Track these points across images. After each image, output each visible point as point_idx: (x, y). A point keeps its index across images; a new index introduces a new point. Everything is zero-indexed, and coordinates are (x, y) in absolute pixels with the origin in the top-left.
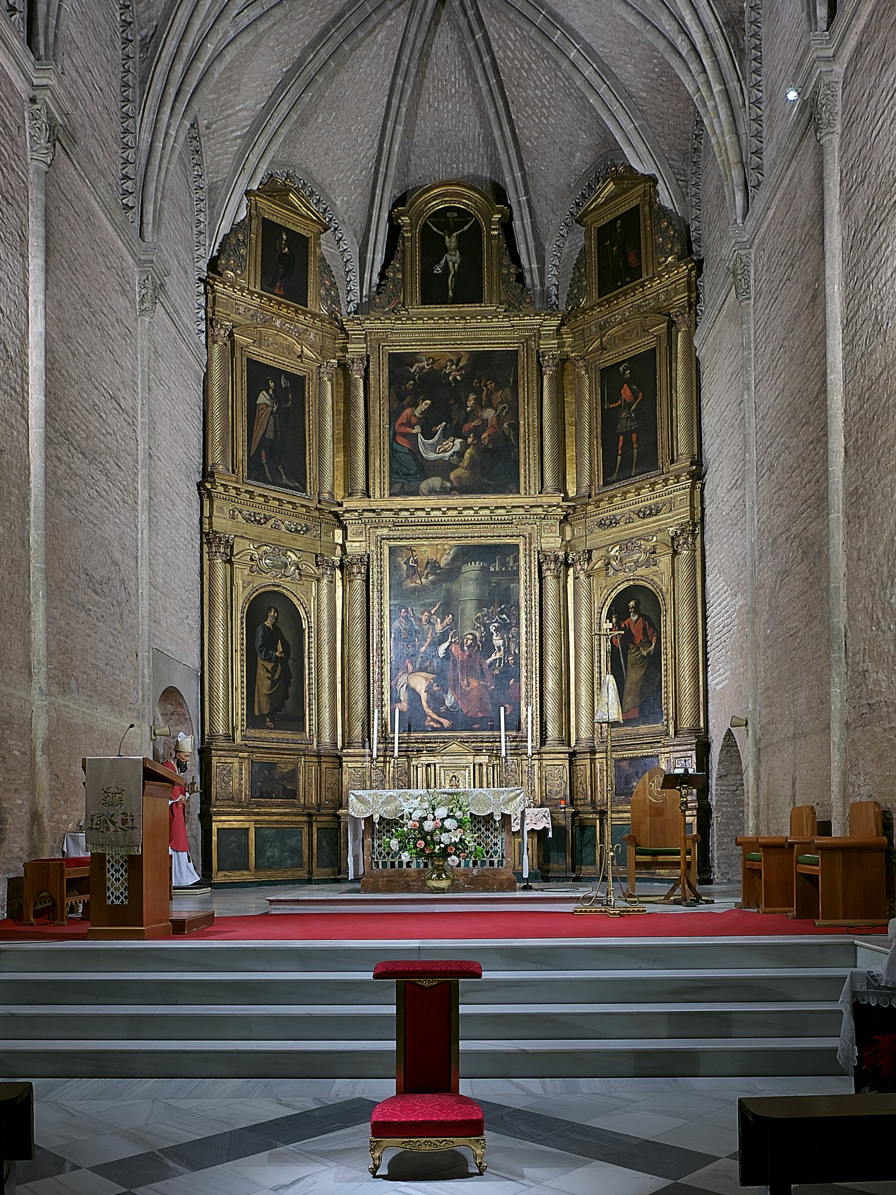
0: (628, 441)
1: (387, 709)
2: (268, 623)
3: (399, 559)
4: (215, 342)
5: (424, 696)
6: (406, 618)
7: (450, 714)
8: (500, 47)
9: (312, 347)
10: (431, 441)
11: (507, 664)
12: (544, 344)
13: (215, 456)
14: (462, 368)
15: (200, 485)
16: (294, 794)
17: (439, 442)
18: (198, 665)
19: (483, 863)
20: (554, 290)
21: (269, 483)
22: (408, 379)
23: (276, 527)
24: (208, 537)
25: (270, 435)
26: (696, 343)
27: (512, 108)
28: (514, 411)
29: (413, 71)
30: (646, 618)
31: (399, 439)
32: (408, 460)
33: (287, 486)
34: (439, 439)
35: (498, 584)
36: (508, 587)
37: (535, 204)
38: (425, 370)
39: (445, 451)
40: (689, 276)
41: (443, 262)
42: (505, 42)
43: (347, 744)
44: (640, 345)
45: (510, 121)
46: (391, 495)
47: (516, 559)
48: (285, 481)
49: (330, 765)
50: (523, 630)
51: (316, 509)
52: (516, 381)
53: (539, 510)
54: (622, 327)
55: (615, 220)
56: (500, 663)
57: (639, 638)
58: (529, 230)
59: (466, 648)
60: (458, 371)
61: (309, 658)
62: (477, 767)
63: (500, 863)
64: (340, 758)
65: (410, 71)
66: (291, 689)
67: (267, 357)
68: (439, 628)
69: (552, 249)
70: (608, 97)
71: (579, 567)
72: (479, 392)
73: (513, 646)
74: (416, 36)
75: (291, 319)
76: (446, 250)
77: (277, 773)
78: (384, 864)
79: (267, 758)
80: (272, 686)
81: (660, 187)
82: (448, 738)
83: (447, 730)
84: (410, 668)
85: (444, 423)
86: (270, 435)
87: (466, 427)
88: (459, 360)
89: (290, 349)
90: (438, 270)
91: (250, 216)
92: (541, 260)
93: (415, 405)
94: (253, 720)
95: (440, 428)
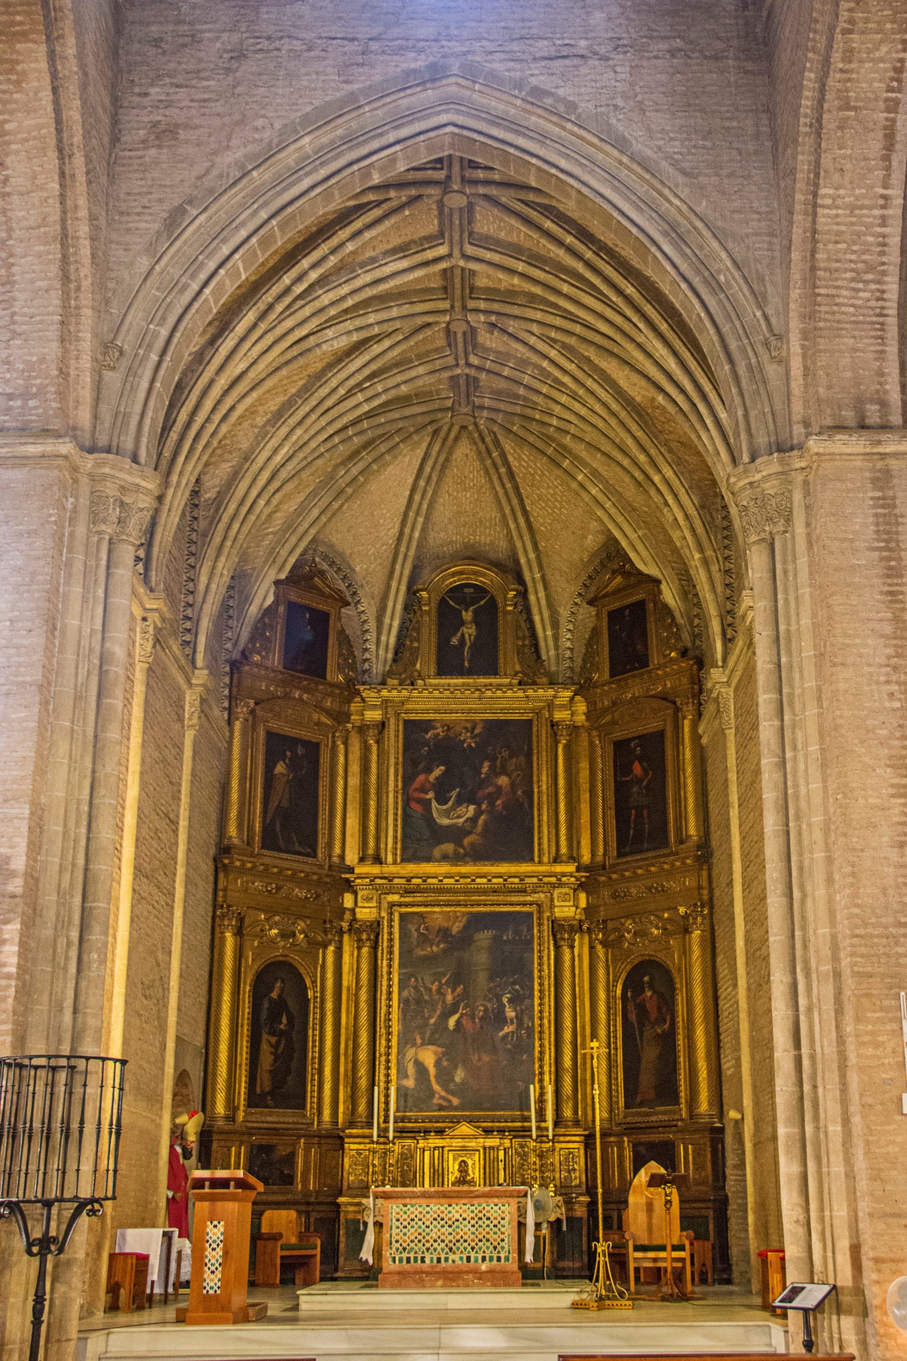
0: (639, 816)
2: (274, 995)
5: (432, 1071)
6: (416, 988)
7: (460, 1091)
11: (520, 1038)
12: (558, 715)
16: (289, 1180)
19: (491, 1259)
20: (568, 654)
21: (280, 850)
22: (423, 746)
25: (285, 804)
26: (700, 731)
27: (527, 502)
29: (434, 478)
30: (661, 995)
31: (414, 805)
37: (549, 577)
39: (459, 817)
43: (352, 1124)
46: (403, 861)
47: (531, 928)
48: (297, 847)
50: (537, 1002)
52: (530, 749)
53: (553, 880)
57: (654, 1014)
58: (543, 602)
63: (507, 1259)
64: (342, 1139)
65: (429, 479)
66: (294, 1065)
68: (449, 998)
69: (563, 623)
70: (613, 511)
73: (526, 1019)
76: (463, 623)
77: (276, 1156)
78: (401, 1260)
79: (266, 1140)
80: (275, 1061)
81: (664, 587)
83: (456, 1109)
84: (419, 1041)
86: (285, 804)
87: (480, 794)
88: (474, 728)
90: (455, 641)
91: (276, 602)
92: (555, 625)
93: (429, 770)
94: (253, 1100)
95: (454, 794)
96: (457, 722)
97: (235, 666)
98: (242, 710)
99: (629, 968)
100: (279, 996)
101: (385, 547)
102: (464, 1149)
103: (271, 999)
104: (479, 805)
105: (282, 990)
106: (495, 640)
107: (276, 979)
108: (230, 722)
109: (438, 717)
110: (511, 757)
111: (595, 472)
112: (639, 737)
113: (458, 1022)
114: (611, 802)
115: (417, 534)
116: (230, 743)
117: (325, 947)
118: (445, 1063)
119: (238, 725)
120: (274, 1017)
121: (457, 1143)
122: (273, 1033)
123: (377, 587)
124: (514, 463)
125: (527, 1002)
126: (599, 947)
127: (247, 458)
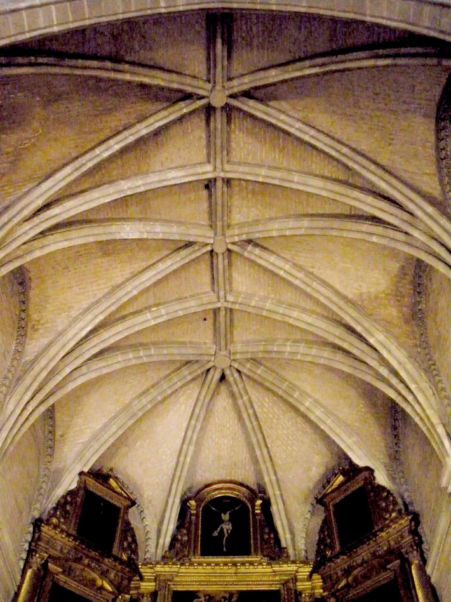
4: (30, 568)
8: (259, 406)
9: (111, 582)
12: (300, 586)
41: (219, 529)
42: (262, 404)
65: (202, 416)
69: (297, 522)
74: (205, 398)
75: (98, 561)
76: (222, 522)
81: (377, 474)
89: (93, 582)
90: (216, 534)
91: (78, 488)
92: (292, 533)
97: (37, 524)
98: (37, 561)
101: (166, 479)
109: (201, 588)
111: (317, 401)
115: (188, 459)
116: (22, 582)
119: (29, 573)
123: (160, 507)
124: (258, 411)
127: (61, 334)
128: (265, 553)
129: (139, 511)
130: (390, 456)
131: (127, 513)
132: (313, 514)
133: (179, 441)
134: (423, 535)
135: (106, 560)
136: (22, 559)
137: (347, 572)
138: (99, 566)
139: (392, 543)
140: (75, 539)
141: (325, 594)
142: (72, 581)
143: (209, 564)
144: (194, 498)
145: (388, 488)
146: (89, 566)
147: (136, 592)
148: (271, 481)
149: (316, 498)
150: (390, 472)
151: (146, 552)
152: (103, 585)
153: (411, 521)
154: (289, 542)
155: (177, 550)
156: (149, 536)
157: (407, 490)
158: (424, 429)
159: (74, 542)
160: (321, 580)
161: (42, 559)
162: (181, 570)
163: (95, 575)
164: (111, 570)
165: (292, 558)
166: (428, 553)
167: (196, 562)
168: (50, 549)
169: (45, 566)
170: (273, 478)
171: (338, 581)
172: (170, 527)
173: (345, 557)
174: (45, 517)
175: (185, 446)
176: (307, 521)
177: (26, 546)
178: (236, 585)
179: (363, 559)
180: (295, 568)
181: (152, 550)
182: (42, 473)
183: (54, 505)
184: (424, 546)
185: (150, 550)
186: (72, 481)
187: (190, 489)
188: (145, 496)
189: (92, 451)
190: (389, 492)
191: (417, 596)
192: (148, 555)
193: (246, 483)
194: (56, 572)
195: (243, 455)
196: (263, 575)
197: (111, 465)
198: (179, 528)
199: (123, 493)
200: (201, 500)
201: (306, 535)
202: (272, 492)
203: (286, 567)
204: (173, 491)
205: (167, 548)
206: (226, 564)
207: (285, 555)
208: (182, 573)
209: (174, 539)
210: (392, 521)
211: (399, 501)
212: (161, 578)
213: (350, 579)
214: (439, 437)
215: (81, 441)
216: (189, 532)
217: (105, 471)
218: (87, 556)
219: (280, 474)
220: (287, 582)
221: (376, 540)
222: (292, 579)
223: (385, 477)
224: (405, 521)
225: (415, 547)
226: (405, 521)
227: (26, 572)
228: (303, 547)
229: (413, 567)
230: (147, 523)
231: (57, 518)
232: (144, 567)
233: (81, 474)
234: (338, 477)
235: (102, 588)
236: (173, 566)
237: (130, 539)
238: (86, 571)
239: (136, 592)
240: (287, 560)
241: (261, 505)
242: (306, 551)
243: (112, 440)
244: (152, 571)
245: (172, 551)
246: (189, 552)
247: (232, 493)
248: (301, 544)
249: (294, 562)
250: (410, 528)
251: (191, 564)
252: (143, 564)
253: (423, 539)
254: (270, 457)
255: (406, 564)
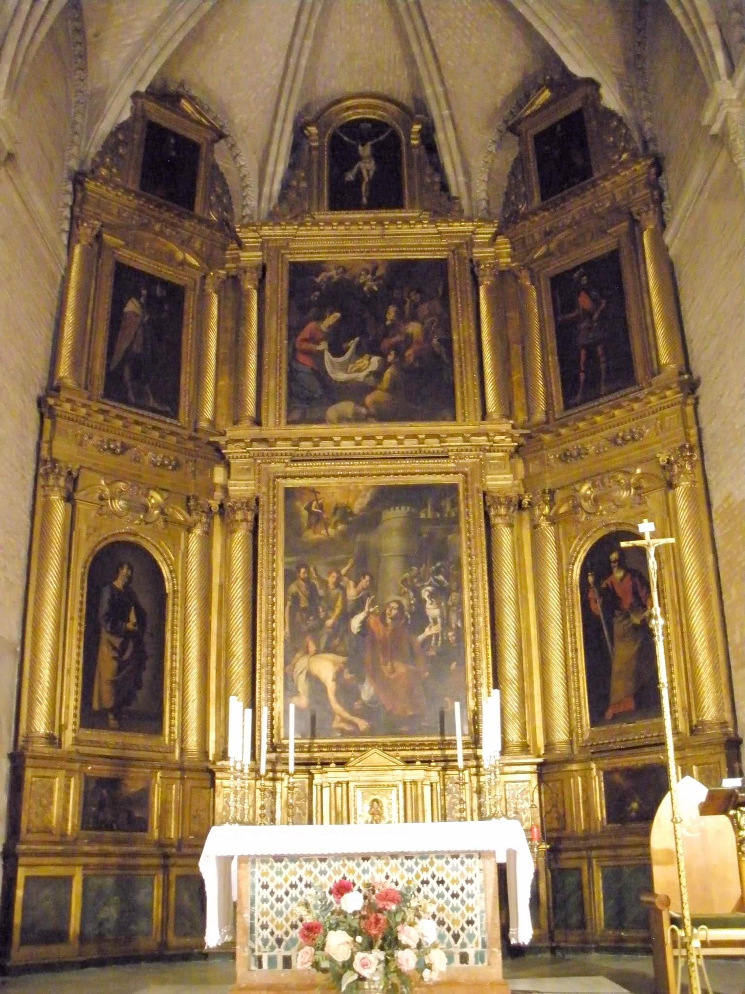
0: (591, 354)
1: (279, 706)
2: (119, 583)
3: (298, 503)
4: (78, 242)
6: (307, 581)
7: (368, 712)
9: (197, 254)
10: (341, 359)
11: (446, 642)
12: (478, 253)
13: (64, 370)
14: (380, 277)
15: (41, 402)
17: (351, 360)
18: (16, 636)
23: (137, 460)
24: (44, 465)
25: (137, 349)
27: (431, 29)
28: (446, 325)
31: (301, 358)
32: (314, 385)
33: (154, 411)
34: (351, 357)
35: (431, 534)
36: (444, 541)
38: (334, 280)
39: (359, 370)
40: (649, 173)
41: (355, 170)
44: (600, 247)
45: (430, 40)
46: (288, 423)
48: (152, 403)
49: (196, 783)
50: (467, 595)
51: (191, 438)
54: (573, 230)
55: (556, 124)
56: (437, 639)
57: (628, 601)
59: (389, 621)
60: (374, 280)
61: (172, 633)
62: (408, 786)
64: (212, 773)
67: (143, 263)
68: (352, 593)
69: (474, 156)
71: (537, 512)
72: (400, 304)
73: (453, 617)
75: (173, 224)
76: (358, 158)
80: (120, 669)
81: (603, 91)
82: (366, 745)
83: (363, 734)
84: (312, 648)
85: (357, 339)
87: (386, 343)
88: (376, 269)
90: (350, 176)
91: (134, 117)
92: (467, 173)
93: (321, 318)
94: (90, 717)
95: (352, 344)
96: (355, 263)
97: (78, 179)
98: (86, 232)
99: (588, 546)
100: (126, 586)
102: (375, 785)
103: (113, 589)
104: (383, 355)
105: (130, 579)
106: (399, 178)
107: (121, 565)
108: (70, 248)
109: (330, 257)
110: (422, 301)
112: (584, 265)
113: (364, 624)
114: (552, 345)
115: (304, 62)
116: (68, 269)
117: (189, 530)
118: (347, 676)
119: (77, 250)
120: (118, 613)
121: (364, 777)
122: (114, 632)
125: (454, 596)
126: (544, 524)
128: (426, 204)
129: (230, 145)
130: (627, 63)
131: (212, 152)
132: (499, 145)
133: (288, 30)
134: (665, 188)
135: (187, 224)
136: (63, 231)
137: (548, 234)
138: (177, 233)
139: (619, 197)
140: (138, 196)
141: (514, 265)
142: (140, 257)
143: (341, 223)
144: (315, 122)
145: (620, 114)
146: (161, 233)
147: (233, 265)
148: (435, 93)
149: (506, 122)
150: (625, 88)
151: (244, 206)
152: (185, 259)
153: (650, 167)
154: (463, 190)
155: (291, 204)
156: (247, 181)
157: (649, 119)
158: (687, 29)
159: (136, 201)
160: (509, 246)
161: (93, 229)
162: (300, 233)
163: (172, 246)
164: (195, 236)
165: (466, 213)
166: (670, 215)
167: (322, 220)
168: (103, 214)
169: (98, 237)
170: (439, 89)
171: (535, 247)
172: (279, 168)
173: (547, 214)
174: (88, 166)
175: (297, 41)
176: (490, 156)
177: (67, 213)
178: (382, 252)
179: (574, 218)
180: (471, 228)
181: (253, 203)
182: (74, 100)
183: (100, 149)
184: (666, 205)
185: (249, 203)
186: (123, 108)
187: (307, 108)
188: (236, 121)
189: (148, 57)
190: (620, 120)
191: (646, 273)
192: (247, 211)
193: (395, 96)
194: (115, 245)
195: (391, 50)
196: (422, 238)
197: (179, 76)
198: (292, 167)
199: (204, 120)
200: (328, 125)
201: (489, 177)
202: (437, 111)
203: (456, 227)
204: (281, 113)
205: (275, 200)
206: (367, 223)
207: (457, 208)
208: (302, 236)
209: (286, 186)
210: (622, 163)
211: (636, 135)
212: (270, 245)
213: (553, 246)
214: (709, 45)
215: (129, 41)
216: (308, 171)
217: (172, 88)
218: (158, 220)
219: (450, 82)
220: (458, 246)
221: (595, 192)
222: (467, 243)
223: (618, 97)
224: (641, 167)
225: (652, 206)
226: (641, 167)
227: (74, 248)
228: (483, 195)
229: (645, 233)
230: (243, 163)
231: (107, 168)
232: (243, 230)
233: (136, 96)
234: (543, 92)
235: (183, 263)
236: (288, 227)
237: (218, 190)
238: (159, 241)
239: (233, 265)
240: (460, 216)
241: (420, 131)
242: (488, 202)
243: (180, 37)
244: (256, 235)
245: (285, 206)
246: (310, 205)
247: (374, 114)
248: (480, 190)
249: (470, 219)
250: (648, 178)
251: (315, 224)
252: (243, 226)
253: (666, 194)
254: (435, 56)
255: (635, 224)
